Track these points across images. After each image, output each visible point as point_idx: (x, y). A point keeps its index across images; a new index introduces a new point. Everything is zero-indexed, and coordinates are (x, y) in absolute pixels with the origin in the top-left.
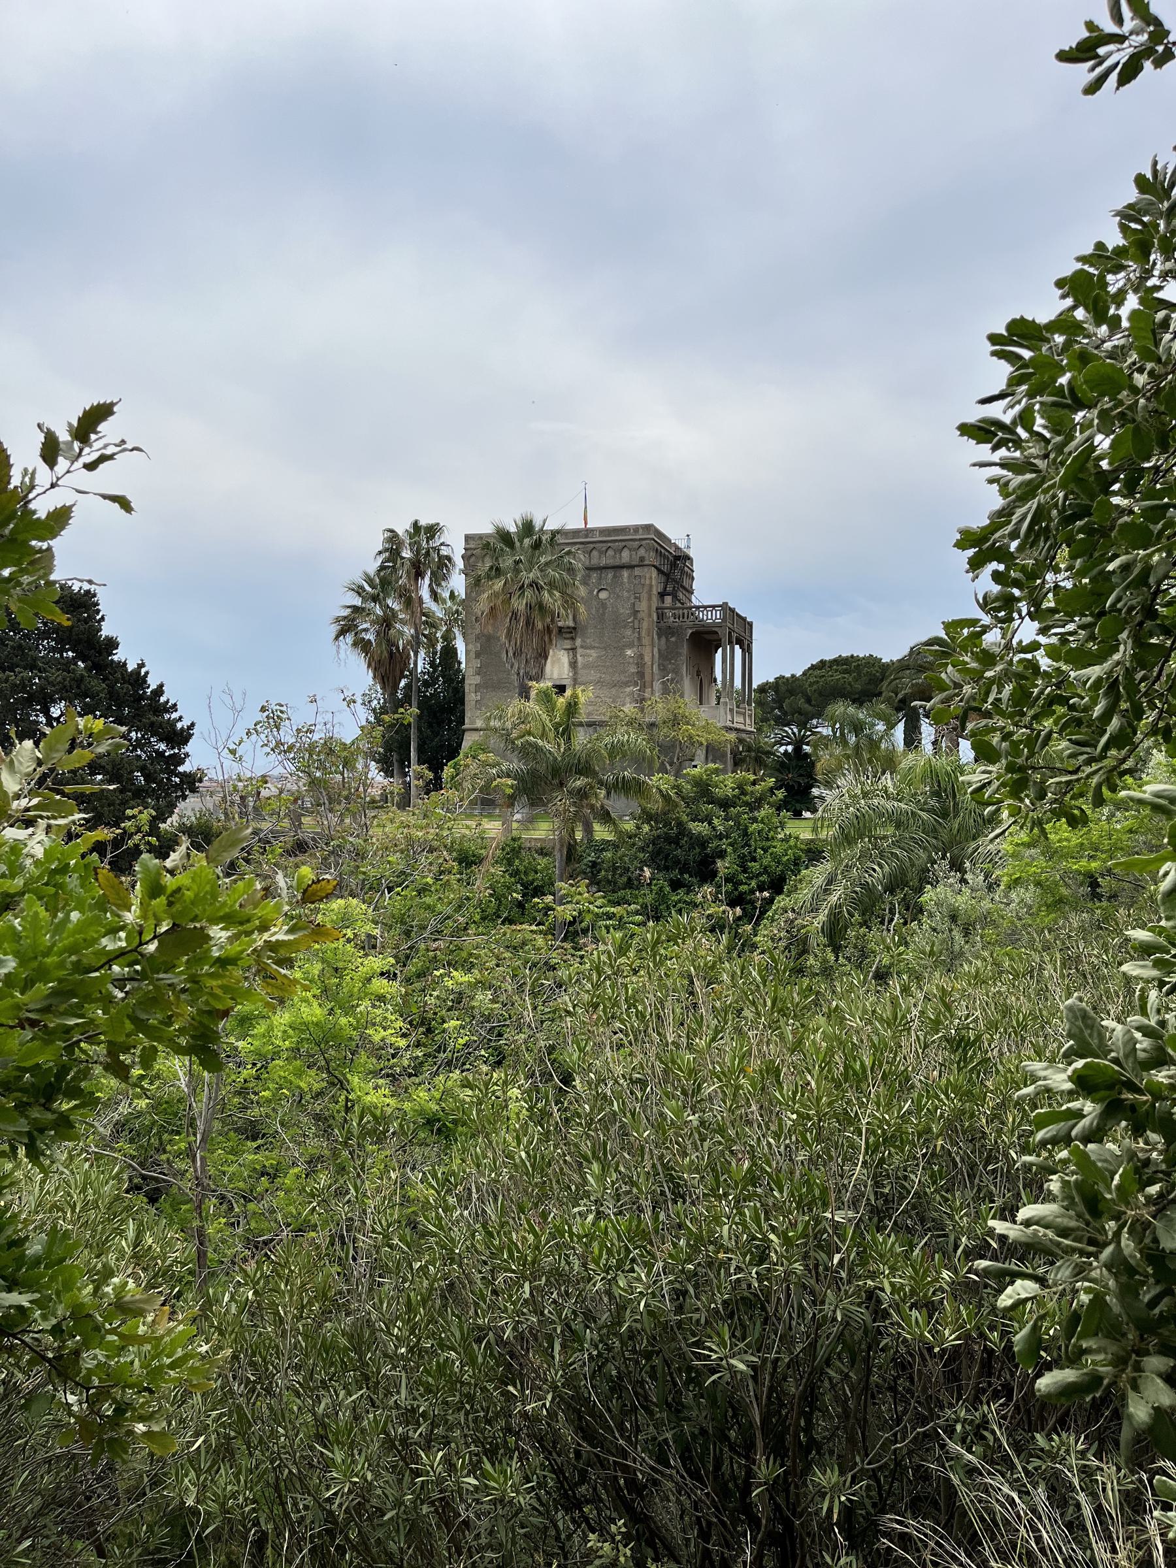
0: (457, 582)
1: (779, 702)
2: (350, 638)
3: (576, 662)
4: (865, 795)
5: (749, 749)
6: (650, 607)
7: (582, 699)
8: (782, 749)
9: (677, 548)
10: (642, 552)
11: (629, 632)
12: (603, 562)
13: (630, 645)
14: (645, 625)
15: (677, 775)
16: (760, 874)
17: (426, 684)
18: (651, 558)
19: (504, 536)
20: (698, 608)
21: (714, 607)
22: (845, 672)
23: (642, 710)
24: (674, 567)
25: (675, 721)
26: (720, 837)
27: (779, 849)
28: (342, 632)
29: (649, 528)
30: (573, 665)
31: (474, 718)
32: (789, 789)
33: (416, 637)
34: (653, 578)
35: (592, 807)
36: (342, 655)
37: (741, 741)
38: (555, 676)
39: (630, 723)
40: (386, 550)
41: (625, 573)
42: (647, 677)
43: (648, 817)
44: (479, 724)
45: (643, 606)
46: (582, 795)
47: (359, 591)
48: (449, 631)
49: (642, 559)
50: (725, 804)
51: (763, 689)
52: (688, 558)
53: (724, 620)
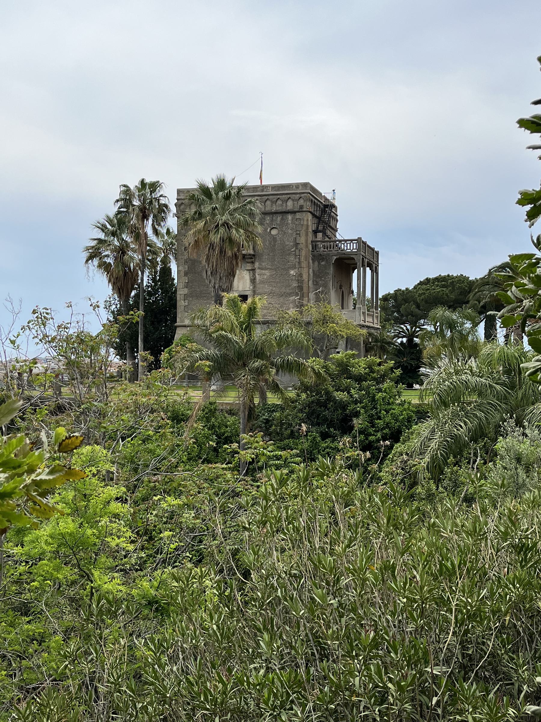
0: (172, 223)
1: (397, 307)
2: (96, 262)
3: (255, 279)
4: (457, 373)
5: (376, 341)
6: (307, 241)
7: (259, 305)
8: (399, 341)
9: (326, 199)
10: (301, 202)
11: (292, 258)
12: (274, 209)
13: (294, 267)
14: (303, 253)
15: (326, 359)
16: (384, 429)
17: (150, 294)
18: (308, 206)
19: (205, 190)
20: (340, 241)
21: (352, 240)
22: (443, 286)
23: (301, 313)
24: (324, 213)
25: (325, 320)
26: (356, 402)
27: (397, 410)
28: (91, 258)
29: (306, 185)
30: (253, 281)
31: (183, 318)
32: (404, 368)
33: (143, 261)
34: (309, 220)
35: (266, 381)
36: (91, 274)
37: (370, 334)
38: (240, 289)
39: (293, 322)
40: (122, 199)
41: (290, 217)
42: (305, 290)
43: (305, 388)
44: (187, 322)
45: (302, 240)
46: (259, 372)
47: (103, 228)
48: (166, 257)
49: (301, 207)
50: (359, 379)
51: (386, 298)
52: (333, 206)
53: (359, 249)
